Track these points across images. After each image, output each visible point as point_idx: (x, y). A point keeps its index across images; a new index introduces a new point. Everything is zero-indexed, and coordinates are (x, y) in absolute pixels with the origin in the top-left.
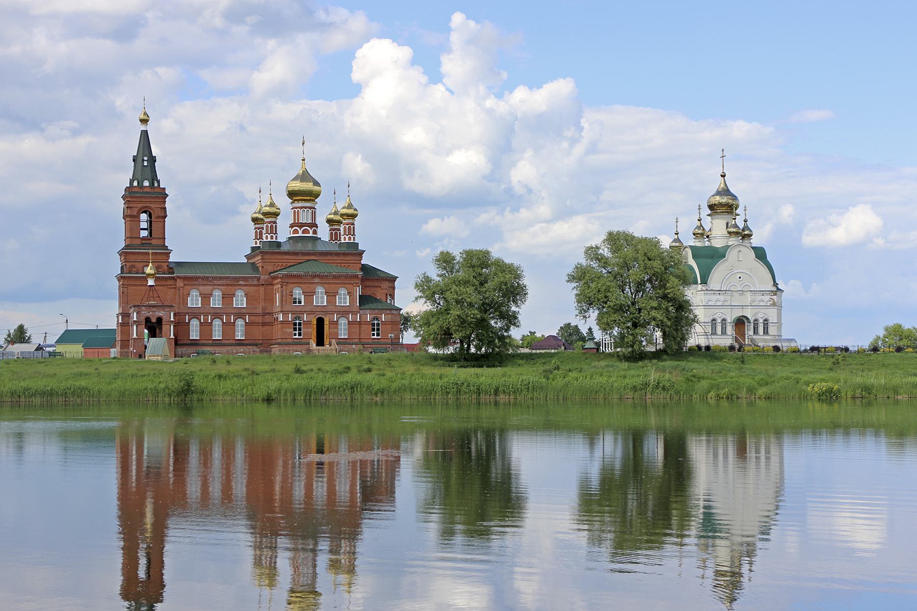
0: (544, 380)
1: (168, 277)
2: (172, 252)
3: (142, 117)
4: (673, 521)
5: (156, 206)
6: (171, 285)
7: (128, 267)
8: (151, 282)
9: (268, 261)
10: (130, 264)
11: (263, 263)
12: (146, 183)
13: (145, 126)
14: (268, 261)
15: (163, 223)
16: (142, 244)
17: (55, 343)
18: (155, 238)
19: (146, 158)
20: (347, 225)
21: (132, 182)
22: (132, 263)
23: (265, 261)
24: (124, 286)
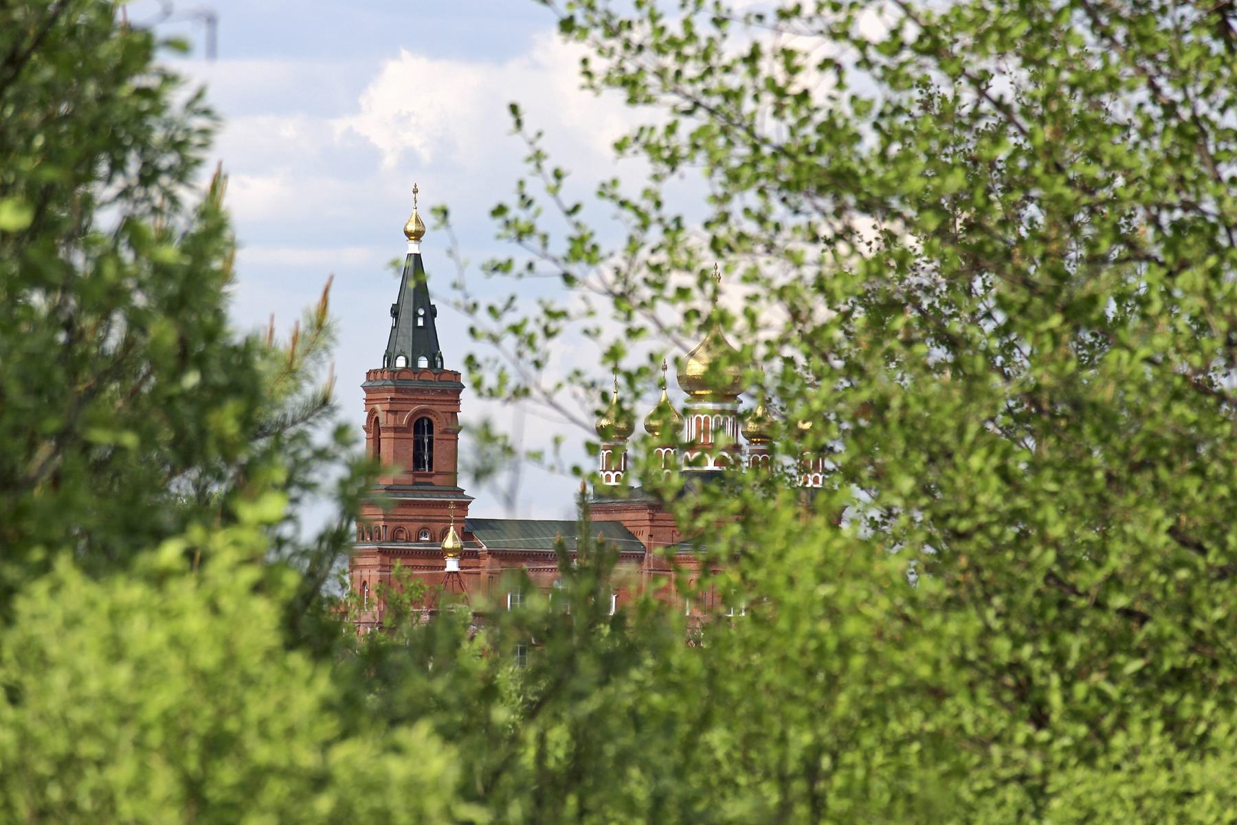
0: (1077, 531)
1: (424, 551)
2: (473, 501)
3: (412, 227)
4: (869, 255)
5: (443, 408)
6: (470, 568)
7: (389, 530)
8: (452, 565)
9: (662, 523)
10: (394, 524)
11: (655, 529)
12: (423, 363)
13: (417, 246)
14: (662, 523)
15: (454, 442)
16: (416, 484)
17: (475, 615)
18: (438, 473)
19: (421, 312)
20: (664, 448)
21: (390, 357)
22: (398, 524)
23: (657, 523)
24: (384, 569)
